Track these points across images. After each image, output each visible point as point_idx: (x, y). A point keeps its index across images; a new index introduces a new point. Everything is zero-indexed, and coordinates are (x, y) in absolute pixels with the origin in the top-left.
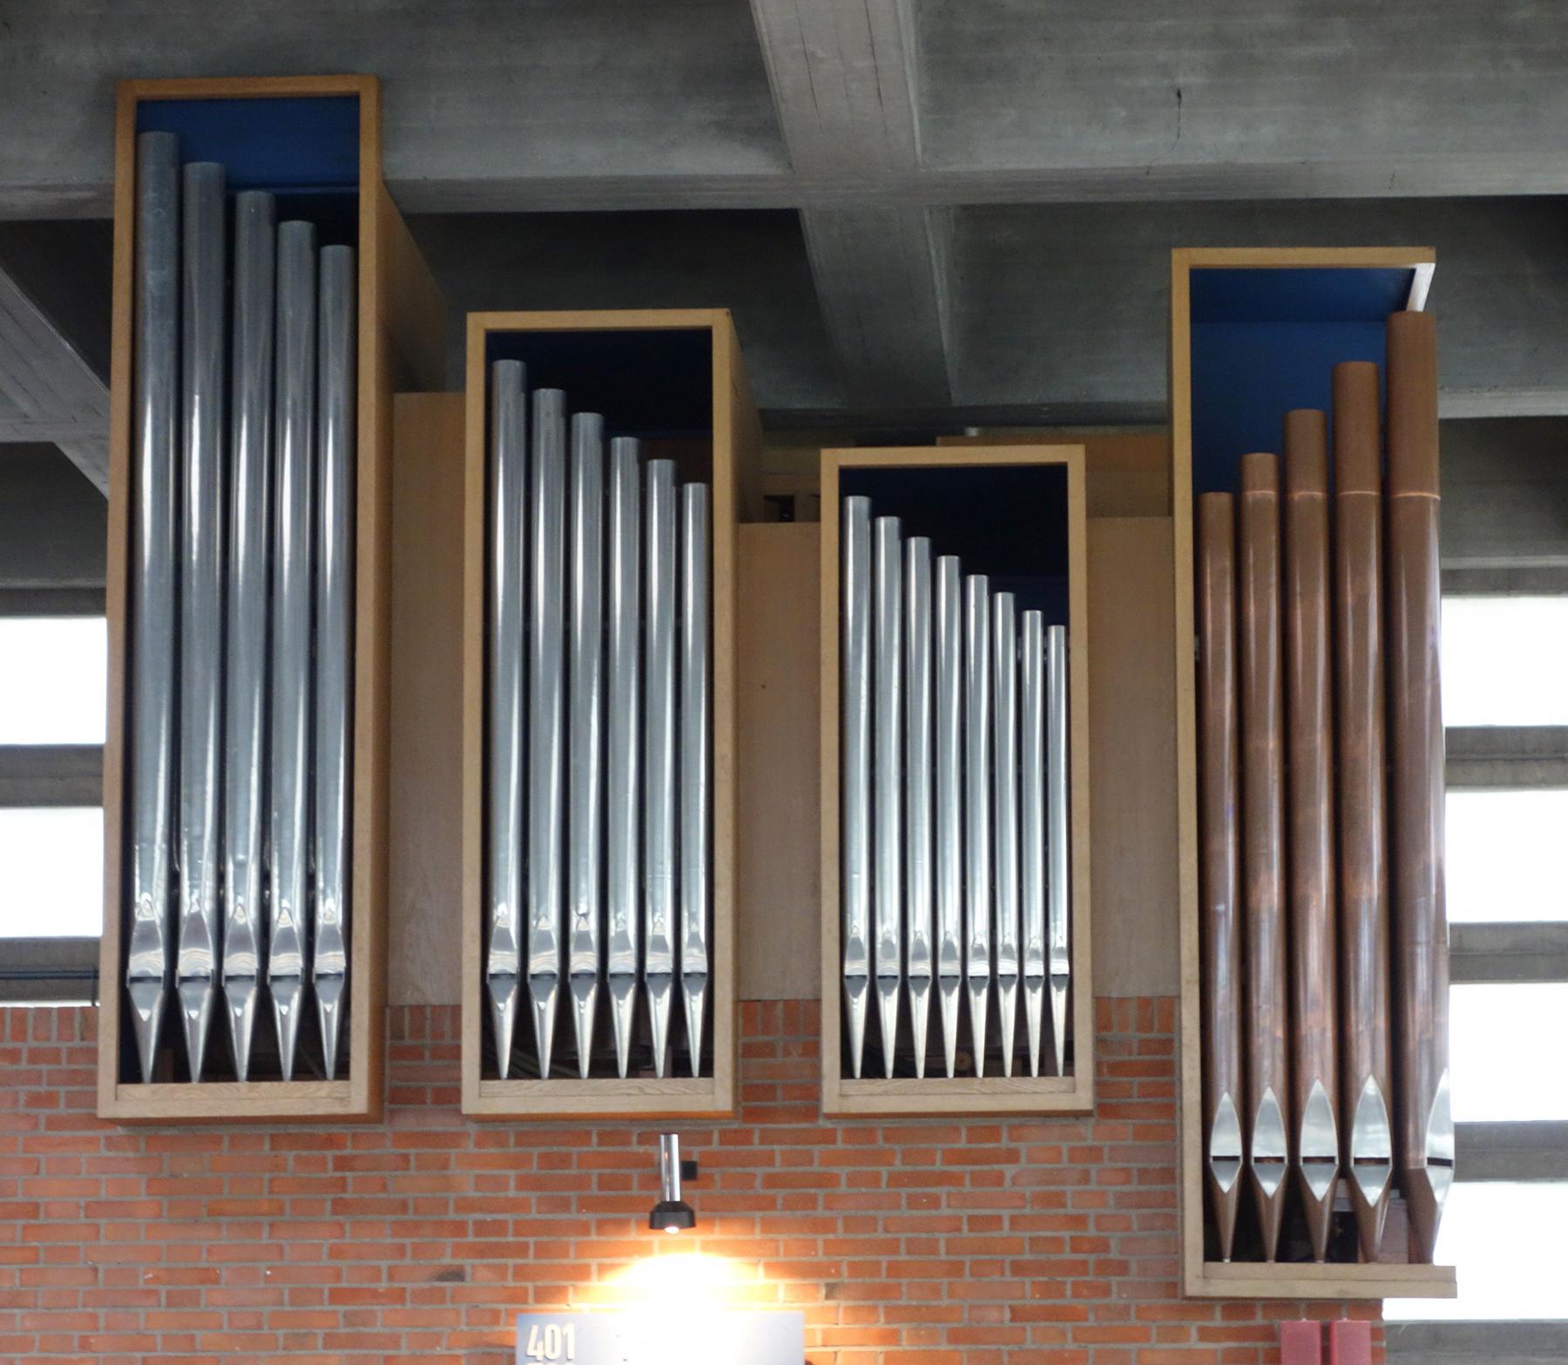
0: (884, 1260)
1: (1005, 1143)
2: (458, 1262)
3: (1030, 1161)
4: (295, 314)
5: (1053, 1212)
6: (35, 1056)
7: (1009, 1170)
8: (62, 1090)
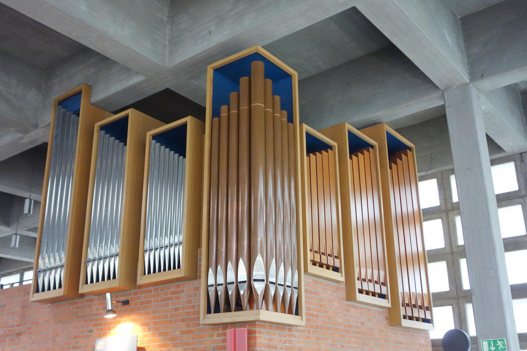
1: (181, 288)
5: (189, 305)
7: (182, 295)
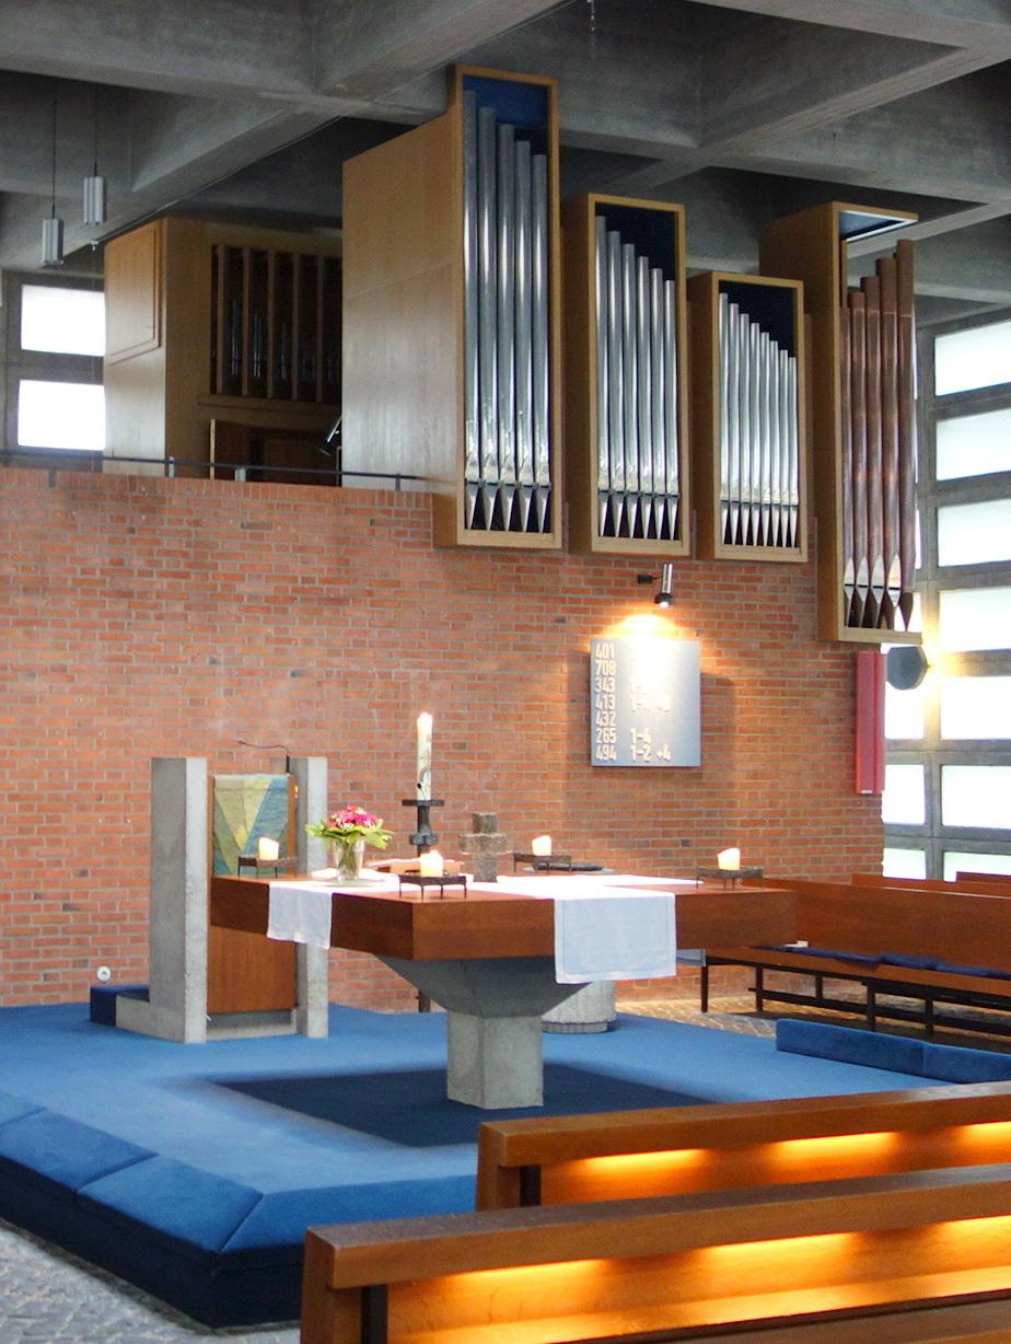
0: (717, 621)
1: (758, 574)
2: (564, 614)
3: (767, 581)
4: (523, 185)
6: (398, 513)
7: (759, 585)
8: (409, 530)
